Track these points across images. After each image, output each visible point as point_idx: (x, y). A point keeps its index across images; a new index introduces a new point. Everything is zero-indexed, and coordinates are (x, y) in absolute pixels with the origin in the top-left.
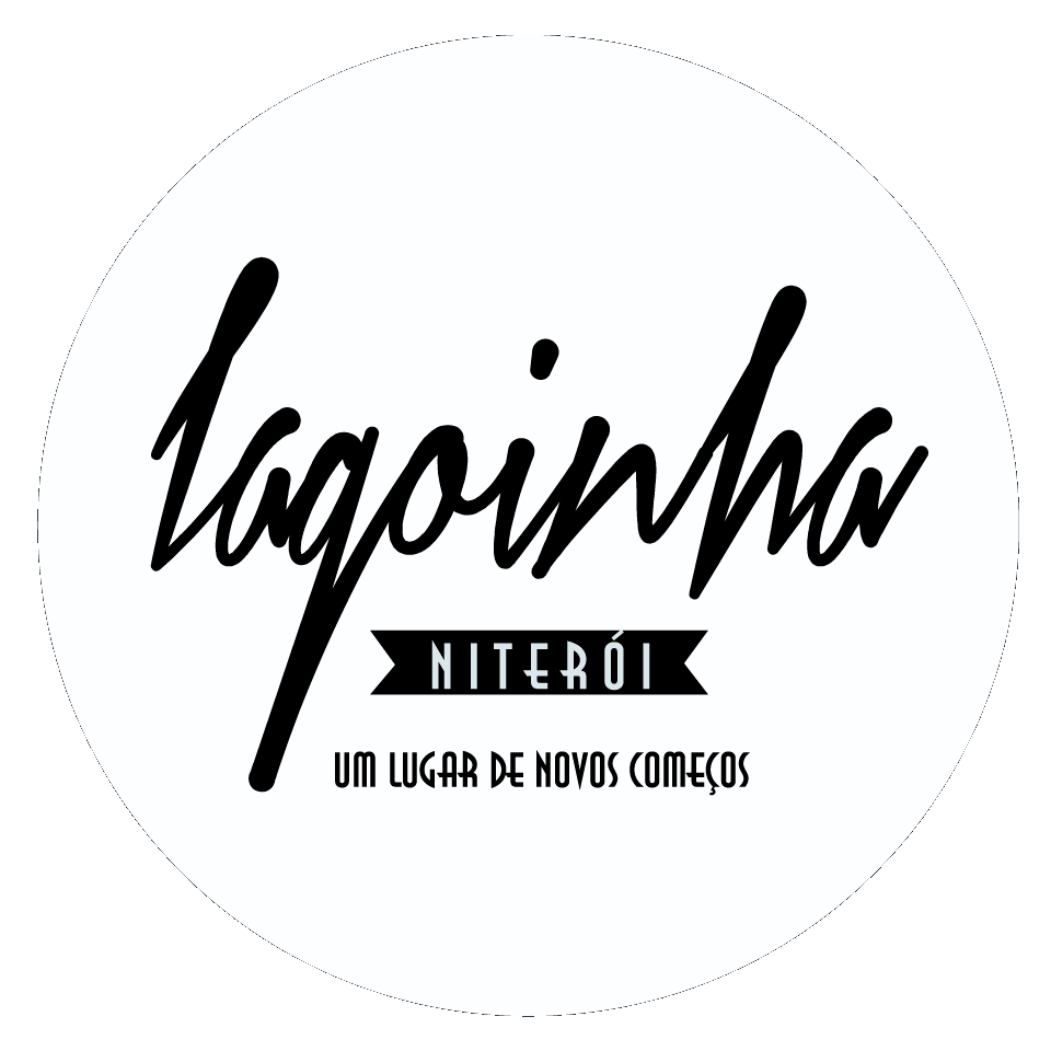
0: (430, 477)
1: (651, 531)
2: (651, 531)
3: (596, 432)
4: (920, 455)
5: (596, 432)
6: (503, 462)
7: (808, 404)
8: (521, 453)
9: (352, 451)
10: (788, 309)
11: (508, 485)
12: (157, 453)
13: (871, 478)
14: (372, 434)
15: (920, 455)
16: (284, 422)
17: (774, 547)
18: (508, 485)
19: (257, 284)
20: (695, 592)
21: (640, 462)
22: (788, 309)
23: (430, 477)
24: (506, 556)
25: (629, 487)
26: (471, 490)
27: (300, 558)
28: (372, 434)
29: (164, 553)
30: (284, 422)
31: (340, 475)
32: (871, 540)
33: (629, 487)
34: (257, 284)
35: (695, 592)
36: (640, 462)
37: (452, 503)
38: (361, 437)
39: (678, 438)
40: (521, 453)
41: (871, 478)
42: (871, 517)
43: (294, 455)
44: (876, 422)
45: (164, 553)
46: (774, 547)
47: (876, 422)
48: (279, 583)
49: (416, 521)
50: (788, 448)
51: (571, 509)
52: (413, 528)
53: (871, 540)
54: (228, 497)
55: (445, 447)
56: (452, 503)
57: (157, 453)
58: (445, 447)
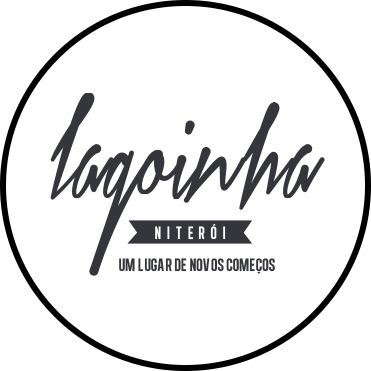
0: (151, 168)
1: (225, 186)
2: (225, 186)
3: (206, 152)
4: (322, 161)
5: (206, 152)
6: (175, 165)
7: (282, 143)
8: (182, 160)
9: (125, 159)
10: (273, 111)
11: (177, 172)
12: (53, 159)
13: (305, 168)
14: (132, 153)
15: (322, 161)
16: (96, 149)
17: (268, 192)
18: (177, 172)
19: (87, 102)
20: (242, 207)
21: (221, 163)
22: (273, 111)
23: (151, 168)
24: (176, 195)
25: (217, 171)
26: (165, 173)
27: (107, 196)
28: (132, 153)
29: (55, 193)
30: (96, 149)
31: (121, 167)
32: (305, 190)
33: (217, 171)
35: (242, 207)
36: (221, 163)
37: (159, 177)
38: (128, 154)
39: (233, 151)
40: (182, 160)
41: (305, 168)
42: (305, 182)
43: (99, 161)
44: (307, 149)
45: (55, 193)
46: (268, 192)
47: (307, 149)
48: (97, 204)
49: (146, 183)
50: (273, 158)
51: (197, 181)
52: (146, 185)
53: (305, 190)
54: (76, 175)
55: (157, 157)
56: (159, 177)
57: (53, 159)
58: (157, 157)
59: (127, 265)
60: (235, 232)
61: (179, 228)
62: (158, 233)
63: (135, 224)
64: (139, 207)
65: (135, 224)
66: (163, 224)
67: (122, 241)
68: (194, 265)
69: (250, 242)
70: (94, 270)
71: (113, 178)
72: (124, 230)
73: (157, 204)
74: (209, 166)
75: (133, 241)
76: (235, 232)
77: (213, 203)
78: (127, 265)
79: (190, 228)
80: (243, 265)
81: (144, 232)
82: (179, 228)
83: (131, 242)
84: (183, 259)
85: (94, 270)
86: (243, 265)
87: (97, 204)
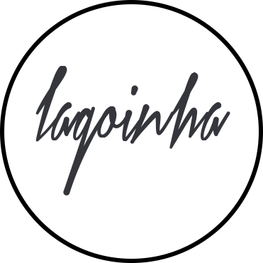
0: (107, 119)
1: (159, 132)
2: (159, 132)
3: (146, 108)
4: (228, 114)
5: (146, 108)
6: (124, 117)
7: (200, 101)
8: (129, 114)
9: (89, 113)
10: (193, 79)
11: (126, 122)
12: (38, 113)
13: (216, 119)
14: (93, 108)
15: (228, 114)
16: (68, 106)
17: (190, 136)
18: (126, 122)
19: (61, 72)
20: (171, 147)
21: (157, 115)
22: (193, 79)
23: (107, 119)
24: (125, 138)
25: (154, 122)
26: (117, 122)
27: (76, 139)
28: (93, 108)
29: (39, 137)
30: (68, 106)
31: (85, 119)
32: (216, 134)
33: (154, 122)
34: (61, 72)
35: (171, 147)
36: (157, 115)
37: (113, 125)
38: (91, 109)
39: (165, 107)
40: (129, 114)
41: (216, 119)
42: (216, 129)
43: (70, 114)
44: (217, 106)
45: (39, 137)
46: (190, 136)
47: (217, 106)
48: (69, 145)
49: (104, 130)
50: (193, 112)
51: (139, 128)
52: (103, 131)
53: (216, 134)
54: (54, 124)
55: (111, 112)
56: (113, 125)
57: (38, 113)
58: (111, 112)
87: (69, 145)
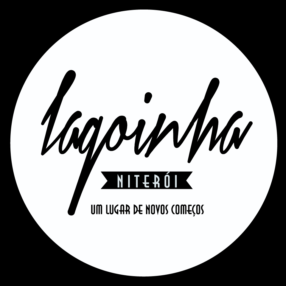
0: (117, 130)
1: (177, 144)
2: (177, 144)
3: (162, 117)
4: (250, 124)
5: (162, 117)
6: (137, 126)
7: (220, 110)
8: (142, 123)
9: (96, 123)
10: (214, 84)
11: (138, 132)
12: (43, 123)
13: (237, 130)
14: (101, 118)
15: (250, 124)
16: (77, 115)
17: (211, 149)
18: (138, 132)
19: (70, 77)
20: (189, 161)
21: (174, 126)
22: (214, 84)
23: (117, 130)
24: (138, 151)
25: (171, 133)
26: (128, 133)
27: (82, 152)
28: (101, 118)
29: (45, 150)
30: (77, 115)
31: (93, 129)
32: (237, 147)
33: (171, 133)
35: (189, 161)
36: (174, 126)
37: (123, 137)
38: (98, 119)
39: (185, 119)
40: (142, 123)
41: (237, 130)
42: (237, 141)
43: (80, 124)
44: (238, 115)
45: (45, 150)
46: (211, 149)
47: (238, 115)
48: (76, 159)
49: (113, 142)
50: (214, 122)
51: (155, 139)
52: (112, 144)
53: (237, 147)
54: (62, 135)
55: (121, 122)
56: (123, 137)
57: (43, 123)
58: (121, 122)
59: (96, 209)
60: (181, 180)
61: (137, 176)
62: (120, 180)
63: (105, 174)
64: (107, 161)
65: (105, 174)
66: (125, 174)
67: (95, 189)
68: (112, 210)
69: (192, 189)
70: (72, 211)
71: (85, 139)
72: (96, 179)
73: (123, 158)
74: (164, 129)
75: (105, 187)
76: (181, 180)
77: (167, 157)
78: (96, 209)
79: (146, 176)
80: (182, 209)
81: (111, 180)
82: (137, 176)
83: (102, 189)
84: (140, 206)
85: (72, 211)
86: (182, 209)
87: (76, 159)
